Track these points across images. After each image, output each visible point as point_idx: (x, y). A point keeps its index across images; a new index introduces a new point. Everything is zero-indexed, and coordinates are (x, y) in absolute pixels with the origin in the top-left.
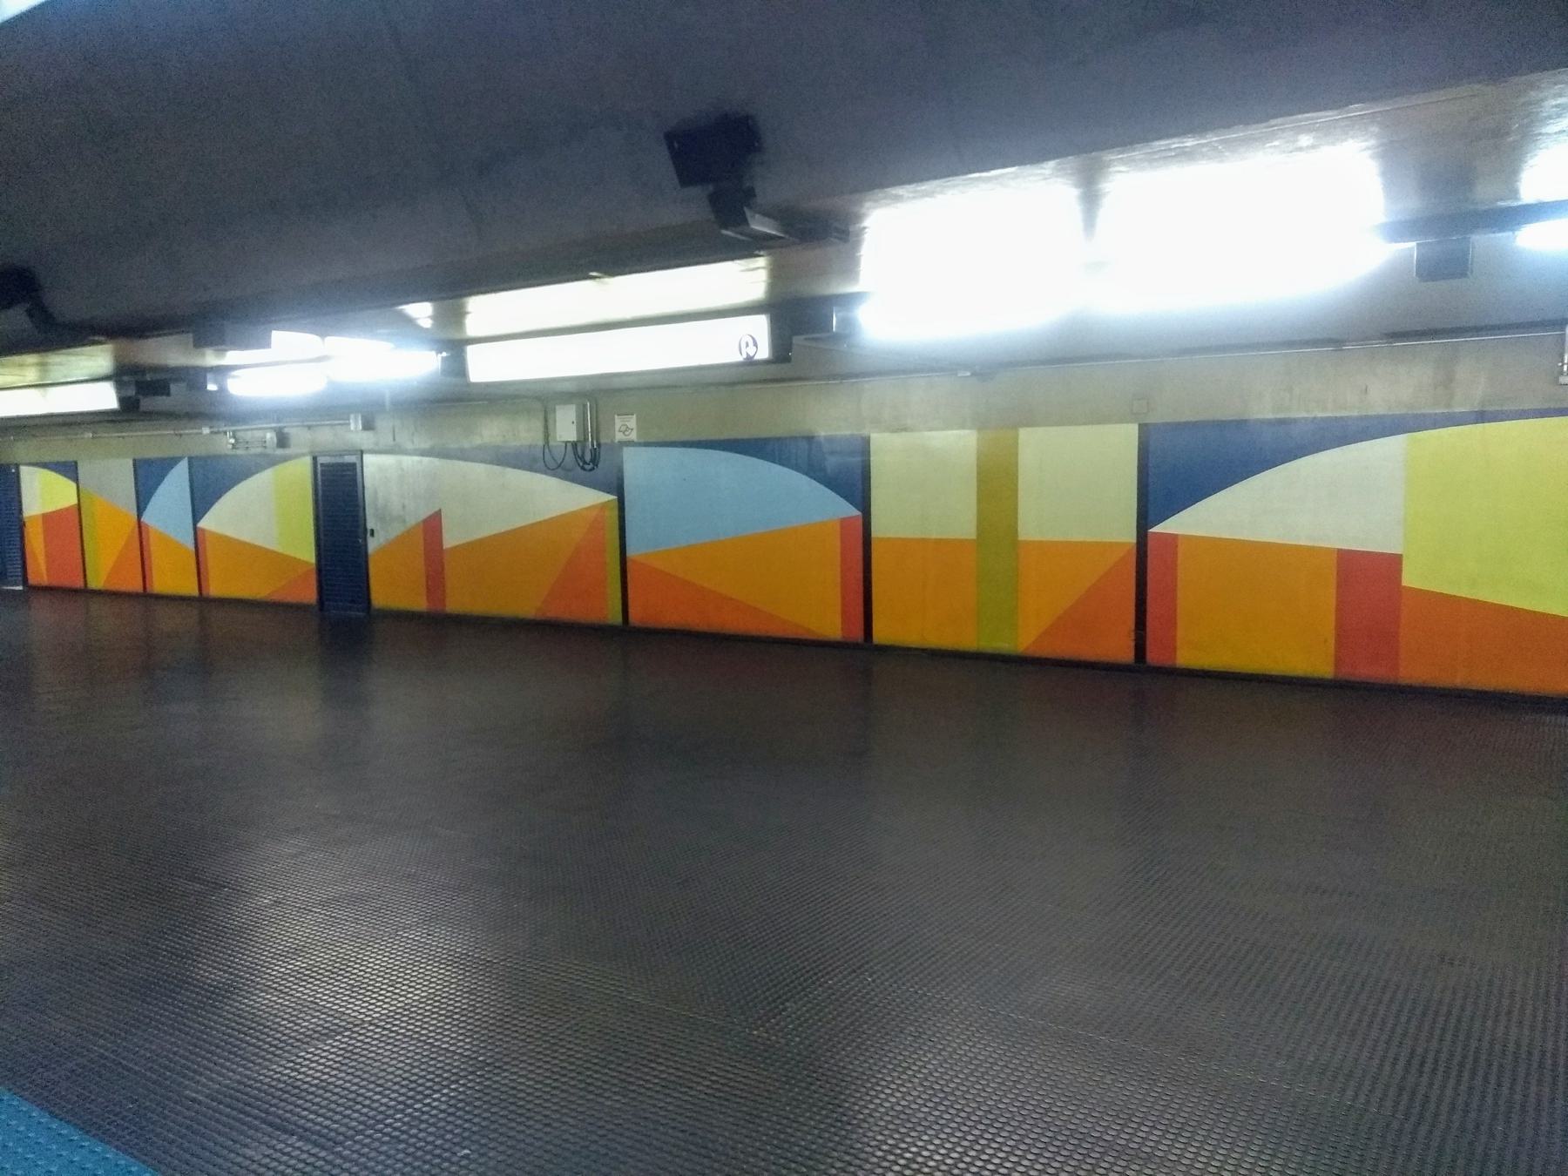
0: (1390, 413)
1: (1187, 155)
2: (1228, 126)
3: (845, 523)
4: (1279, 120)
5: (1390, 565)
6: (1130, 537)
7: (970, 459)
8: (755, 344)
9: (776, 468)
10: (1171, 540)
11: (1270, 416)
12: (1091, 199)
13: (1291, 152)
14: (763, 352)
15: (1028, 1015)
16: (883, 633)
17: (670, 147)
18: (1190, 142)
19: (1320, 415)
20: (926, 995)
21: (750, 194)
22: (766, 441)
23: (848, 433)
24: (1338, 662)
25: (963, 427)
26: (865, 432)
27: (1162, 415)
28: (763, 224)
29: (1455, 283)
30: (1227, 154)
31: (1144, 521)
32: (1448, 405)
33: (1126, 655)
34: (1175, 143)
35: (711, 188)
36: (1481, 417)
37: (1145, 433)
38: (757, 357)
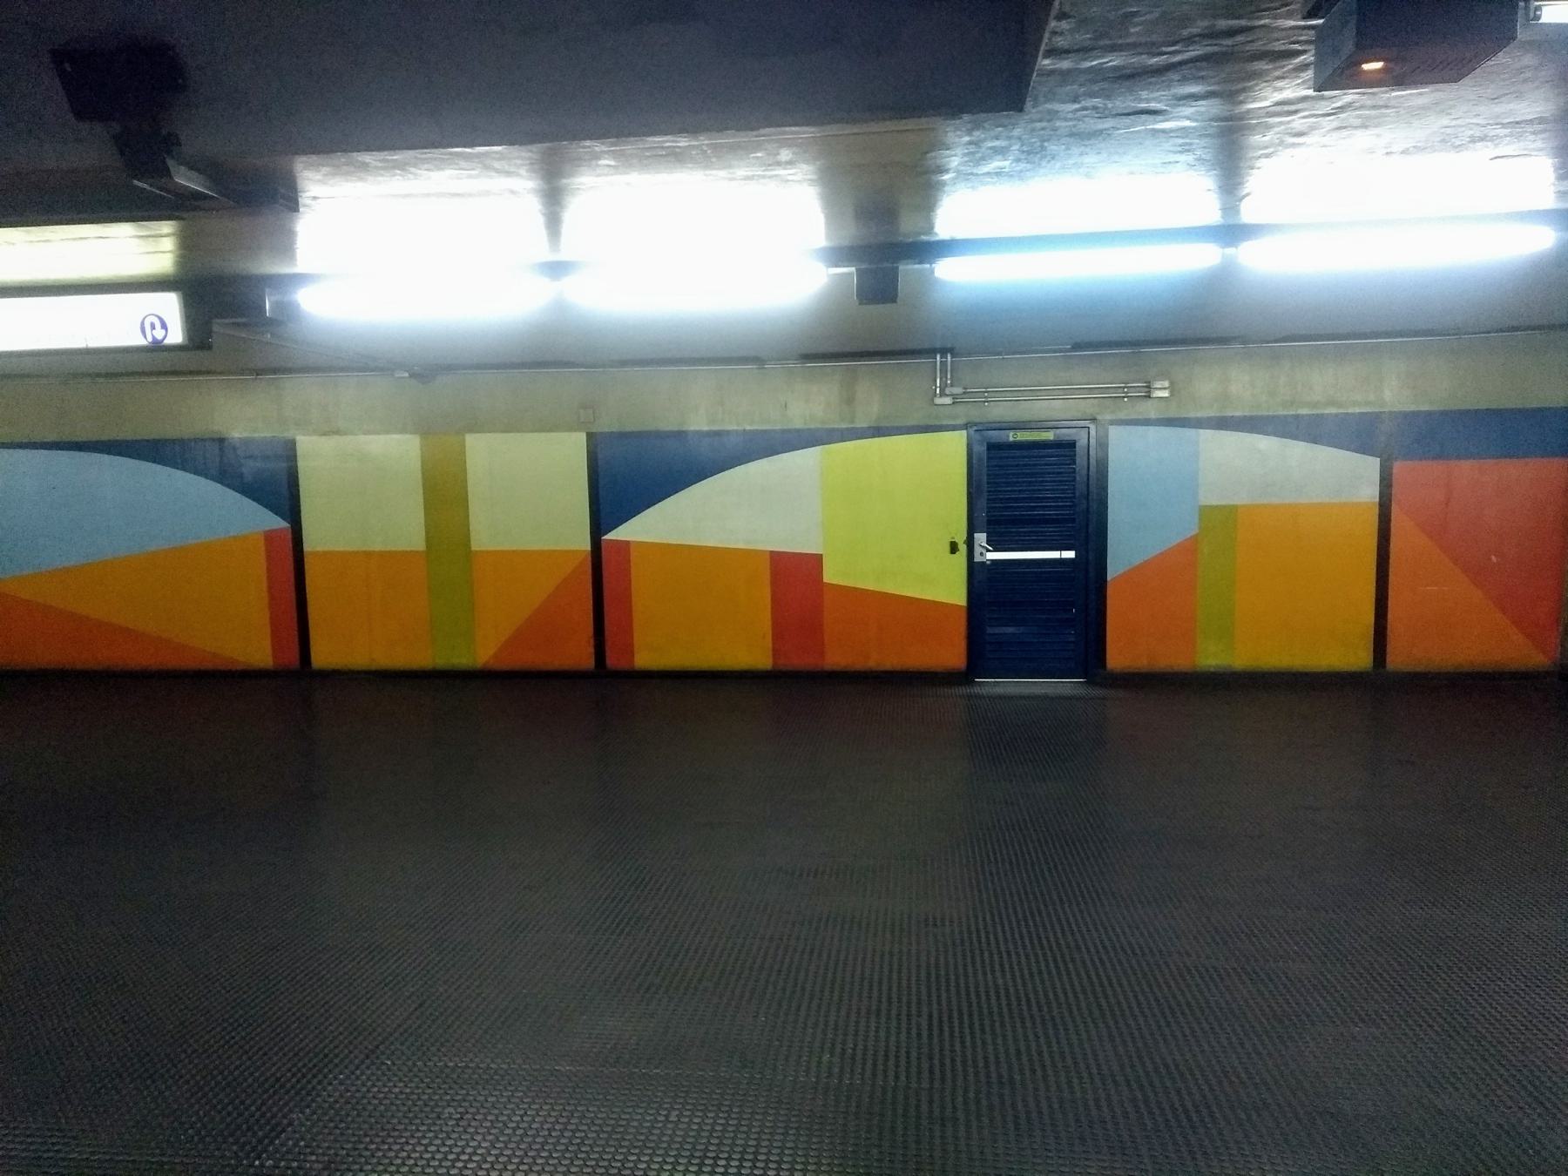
0: (806, 427)
1: (677, 158)
2: (722, 128)
3: (270, 537)
4: (767, 130)
5: (815, 562)
6: (585, 545)
7: (414, 463)
8: (164, 326)
9: (179, 474)
10: (624, 546)
11: (706, 428)
12: (553, 198)
13: (769, 165)
14: (176, 335)
15: (631, 1067)
16: (324, 654)
17: (62, 74)
18: (683, 142)
19: (748, 428)
20: (447, 1066)
21: (170, 143)
22: (182, 443)
23: (268, 434)
24: (776, 652)
25: (403, 431)
26: (288, 435)
27: (606, 425)
28: (189, 179)
29: (889, 306)
30: (714, 160)
31: (598, 528)
32: (853, 422)
33: (587, 661)
34: (668, 141)
35: (116, 127)
36: (878, 431)
37: (593, 442)
38: (167, 342)
